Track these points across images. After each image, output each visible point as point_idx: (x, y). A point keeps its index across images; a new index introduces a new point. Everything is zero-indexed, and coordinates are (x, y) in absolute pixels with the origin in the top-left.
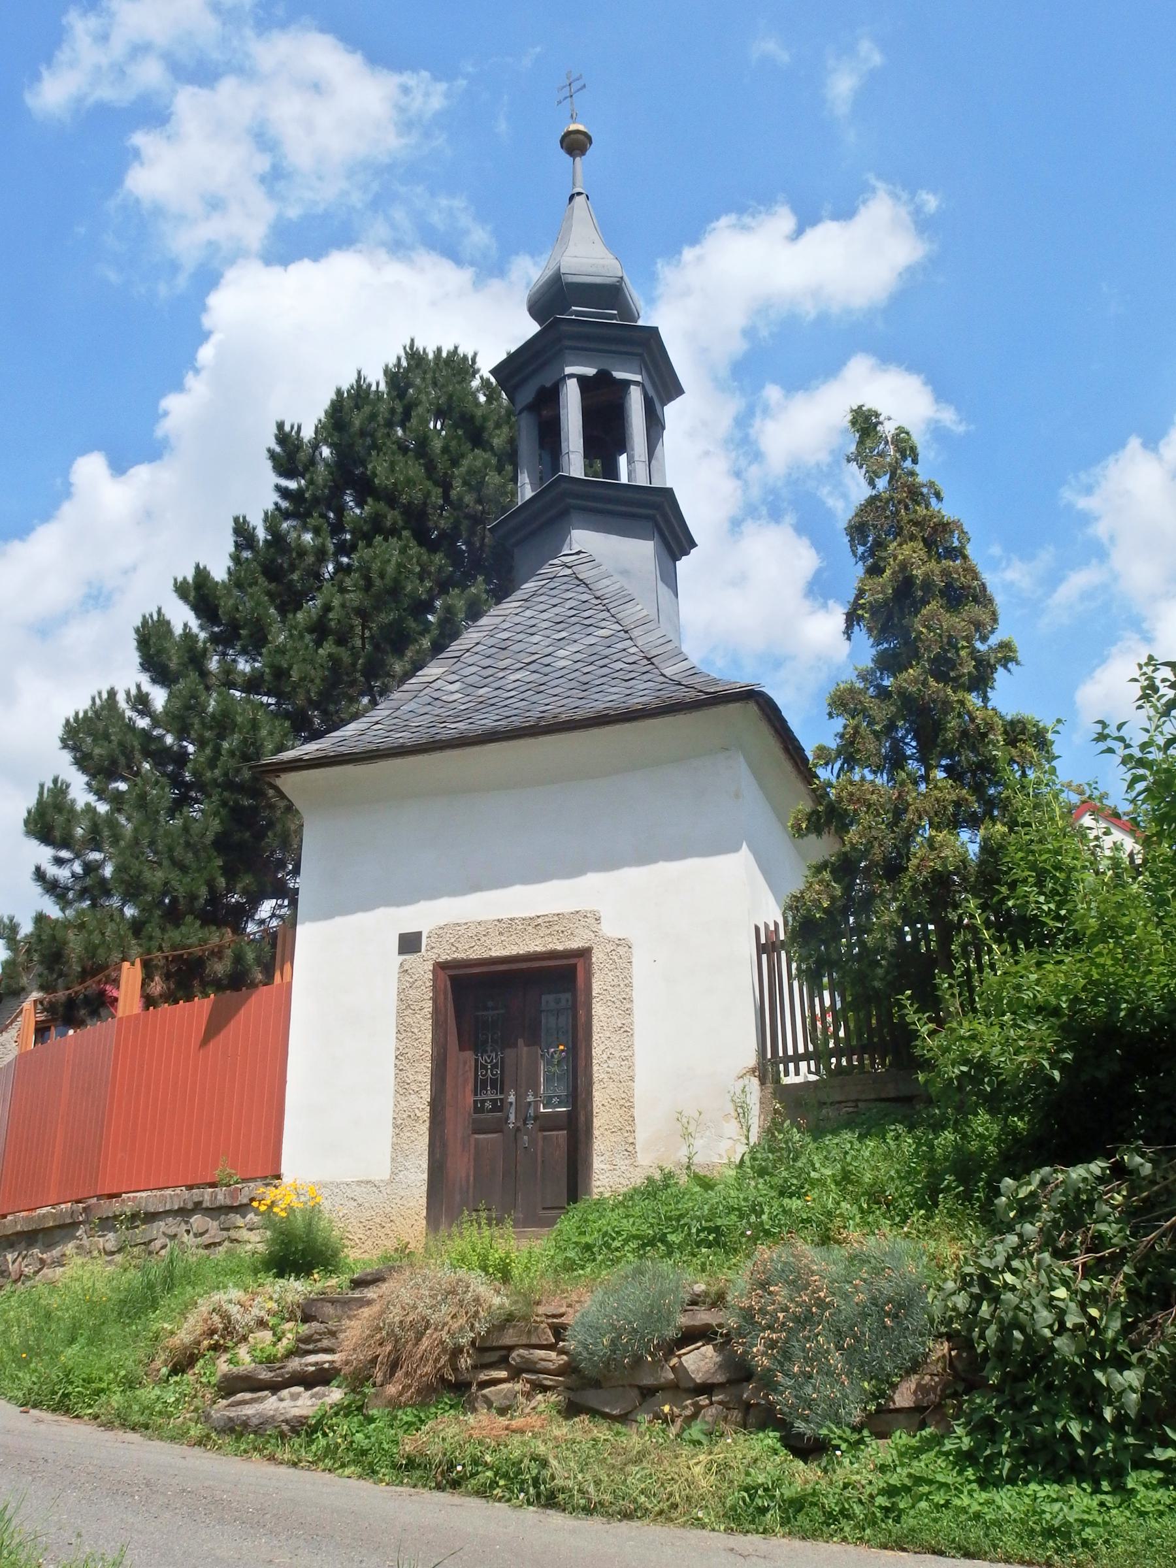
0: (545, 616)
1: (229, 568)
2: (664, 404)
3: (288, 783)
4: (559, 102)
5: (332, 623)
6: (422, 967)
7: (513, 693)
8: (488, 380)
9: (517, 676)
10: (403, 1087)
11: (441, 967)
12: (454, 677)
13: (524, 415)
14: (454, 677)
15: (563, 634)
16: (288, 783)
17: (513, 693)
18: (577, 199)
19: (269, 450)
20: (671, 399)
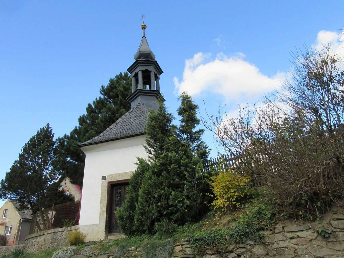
0: (133, 115)
1: (3, 180)
2: (159, 75)
3: (82, 149)
4: (141, 20)
5: (18, 202)
6: (106, 182)
7: (138, 116)
8: (91, 106)
9: (126, 127)
10: (101, 205)
11: (109, 182)
12: (115, 127)
13: (133, 78)
14: (115, 127)
15: (136, 119)
16: (82, 149)
17: (138, 116)
18: (144, 37)
19: (38, 131)
20: (161, 74)
